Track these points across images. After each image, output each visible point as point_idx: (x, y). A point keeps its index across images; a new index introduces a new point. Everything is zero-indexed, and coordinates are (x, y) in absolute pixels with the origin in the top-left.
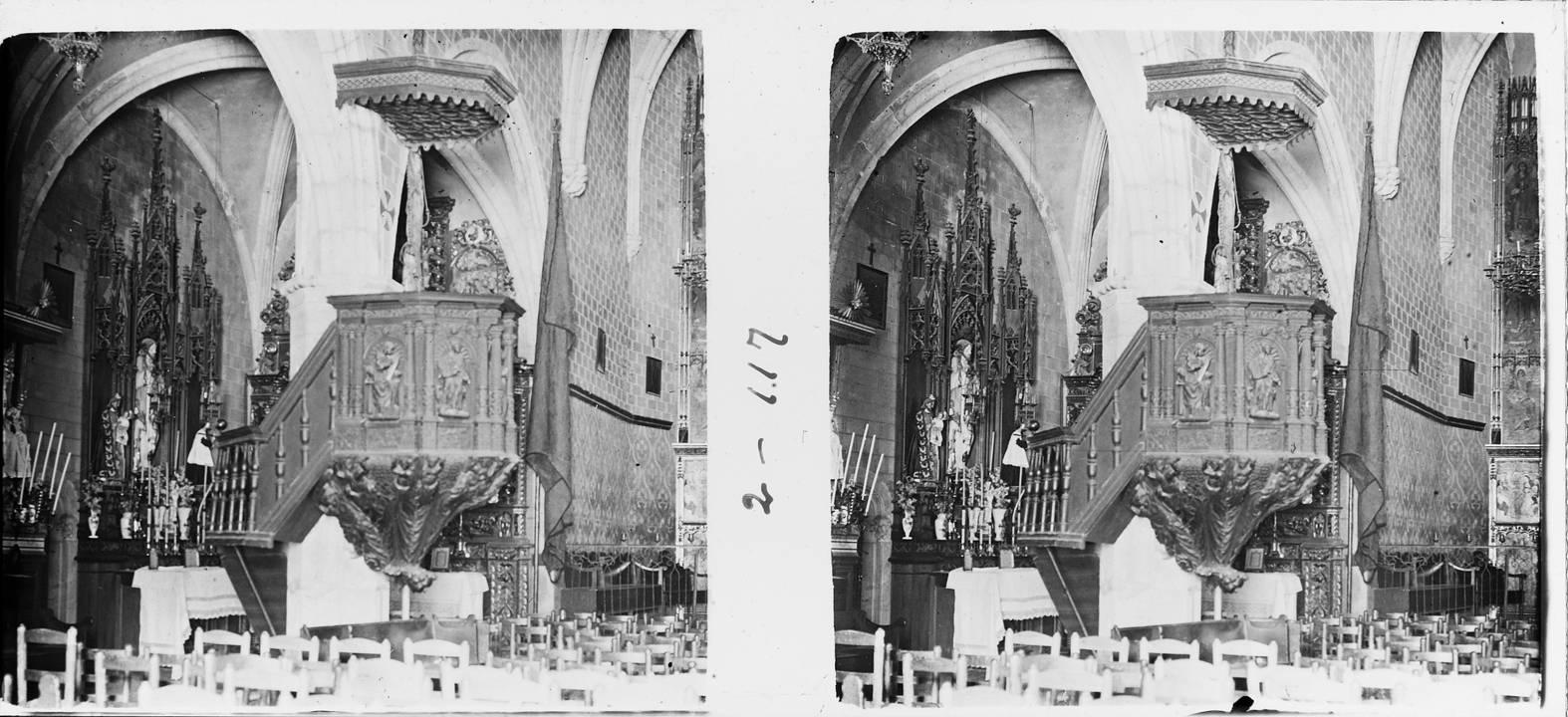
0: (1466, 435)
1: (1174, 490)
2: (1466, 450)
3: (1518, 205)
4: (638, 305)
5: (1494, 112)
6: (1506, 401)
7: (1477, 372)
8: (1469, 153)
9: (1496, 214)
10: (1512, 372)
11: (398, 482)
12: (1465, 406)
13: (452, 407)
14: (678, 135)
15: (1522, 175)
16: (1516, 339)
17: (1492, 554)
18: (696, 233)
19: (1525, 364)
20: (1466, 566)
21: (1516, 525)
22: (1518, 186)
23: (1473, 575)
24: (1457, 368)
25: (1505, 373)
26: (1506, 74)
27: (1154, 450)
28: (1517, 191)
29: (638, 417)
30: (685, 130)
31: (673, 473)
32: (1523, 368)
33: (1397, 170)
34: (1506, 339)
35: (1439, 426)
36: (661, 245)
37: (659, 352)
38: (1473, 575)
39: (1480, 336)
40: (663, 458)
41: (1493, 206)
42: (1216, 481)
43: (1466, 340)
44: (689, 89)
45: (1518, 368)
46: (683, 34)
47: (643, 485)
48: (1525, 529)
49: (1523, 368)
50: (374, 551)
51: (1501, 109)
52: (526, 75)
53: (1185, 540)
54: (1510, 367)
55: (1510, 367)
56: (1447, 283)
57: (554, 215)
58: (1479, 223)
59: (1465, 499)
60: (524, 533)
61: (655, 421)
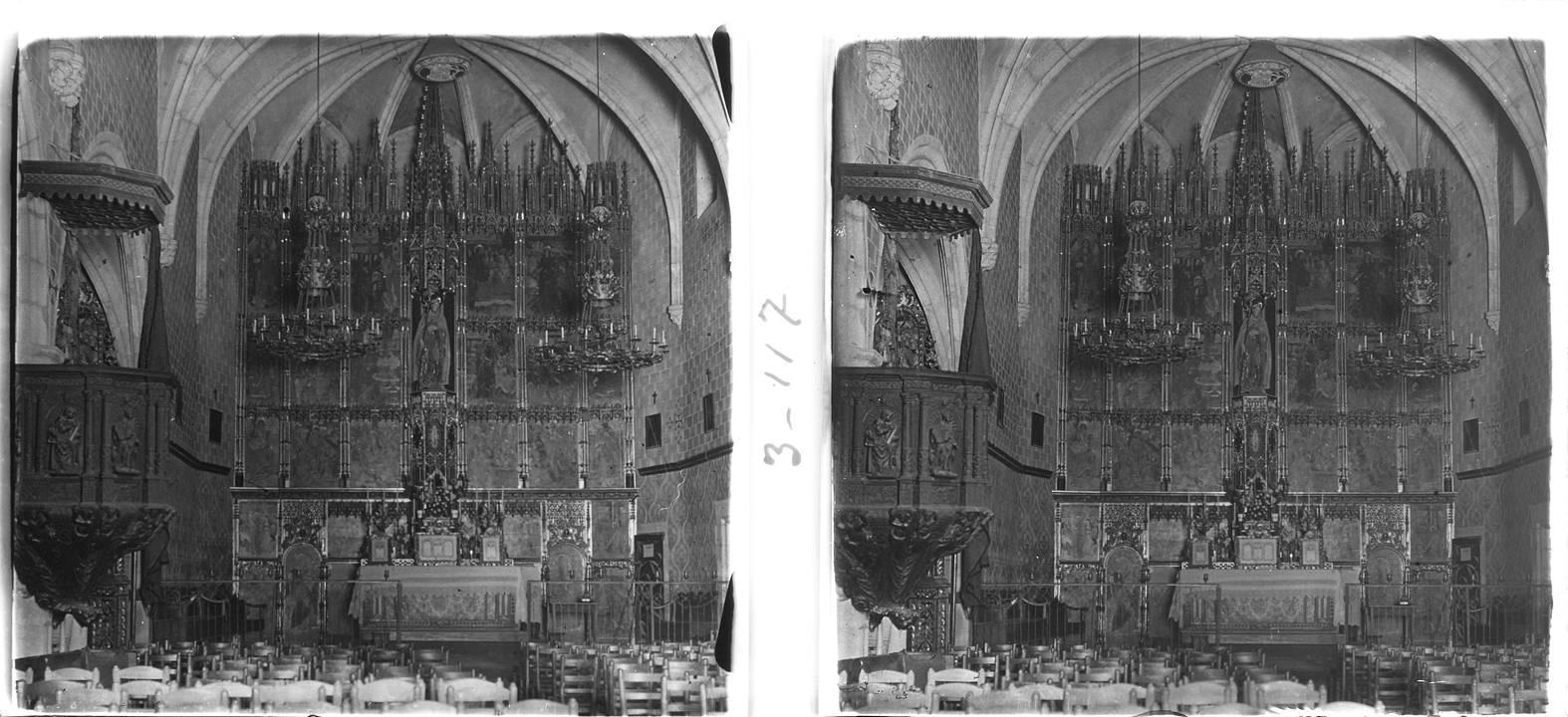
0: (1037, 482)
1: (861, 539)
2: (1036, 497)
3: (259, 273)
4: (204, 362)
5: (1061, 192)
6: (1070, 452)
7: (224, 422)
8: (1041, 228)
9: (1063, 283)
10: (1076, 425)
11: (78, 530)
12: (1036, 455)
13: (126, 466)
14: (236, 211)
15: (1085, 250)
16: (1078, 396)
17: (1057, 592)
18: (250, 300)
19: (265, 415)
20: (1037, 601)
21: (1078, 563)
22: (1081, 260)
23: (1045, 610)
24: (1029, 421)
25: (1068, 427)
26: (249, 155)
27: (28, 500)
28: (259, 260)
29: (1025, 467)
30: (1063, 212)
31: (1052, 517)
32: (1085, 422)
33: (175, 242)
34: (1070, 396)
35: (1014, 473)
36: (1044, 313)
37: (1041, 408)
38: (1045, 610)
39: (1048, 393)
40: (1044, 504)
41: (1059, 275)
42: (86, 528)
43: (215, 392)
44: (244, 171)
45: (1081, 422)
46: (713, 135)
47: (1028, 529)
48: (1087, 567)
49: (1085, 422)
50: (864, 594)
51: (1066, 191)
52: (137, 161)
53: (865, 583)
54: (1074, 421)
55: (1074, 421)
56: (1023, 343)
57: (975, 289)
58: (1048, 291)
59: (1035, 540)
60: (943, 574)
61: (1039, 470)
